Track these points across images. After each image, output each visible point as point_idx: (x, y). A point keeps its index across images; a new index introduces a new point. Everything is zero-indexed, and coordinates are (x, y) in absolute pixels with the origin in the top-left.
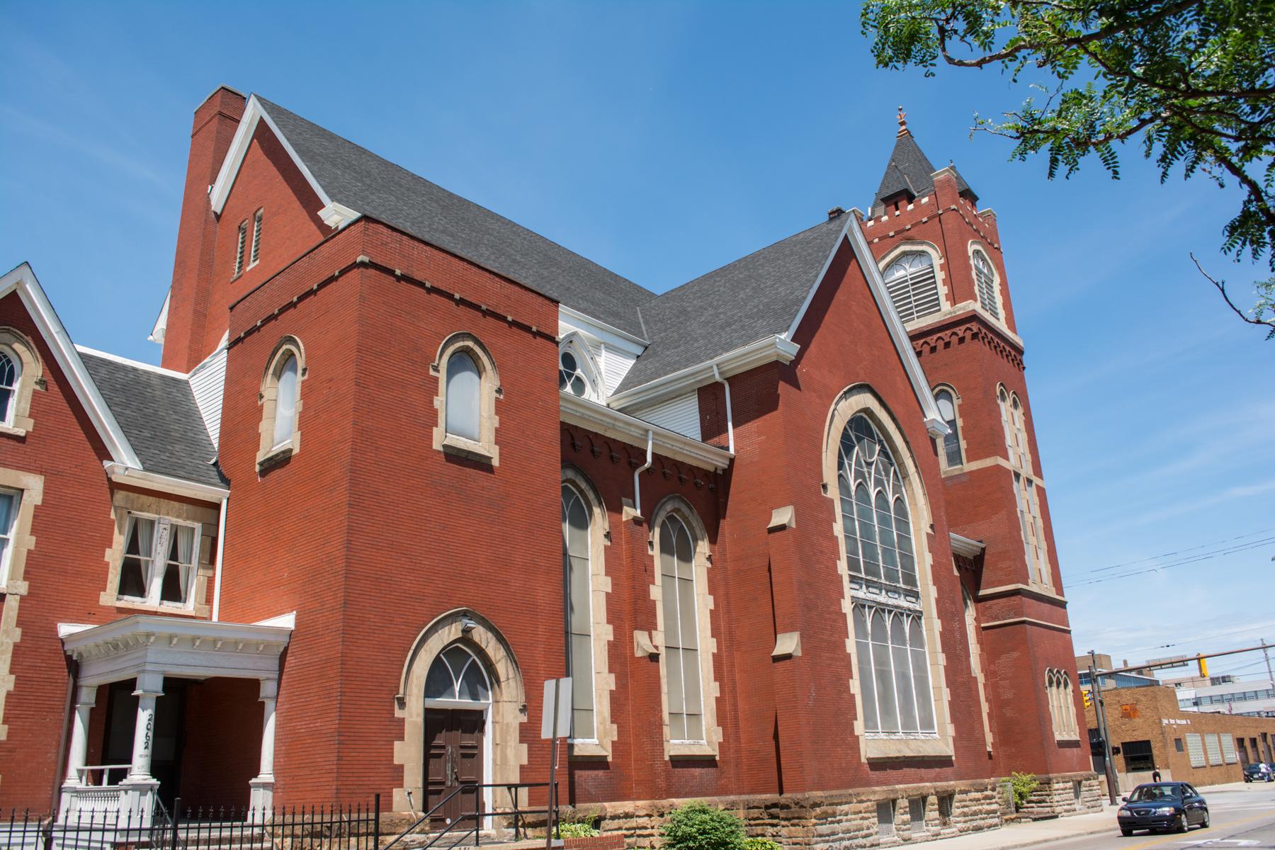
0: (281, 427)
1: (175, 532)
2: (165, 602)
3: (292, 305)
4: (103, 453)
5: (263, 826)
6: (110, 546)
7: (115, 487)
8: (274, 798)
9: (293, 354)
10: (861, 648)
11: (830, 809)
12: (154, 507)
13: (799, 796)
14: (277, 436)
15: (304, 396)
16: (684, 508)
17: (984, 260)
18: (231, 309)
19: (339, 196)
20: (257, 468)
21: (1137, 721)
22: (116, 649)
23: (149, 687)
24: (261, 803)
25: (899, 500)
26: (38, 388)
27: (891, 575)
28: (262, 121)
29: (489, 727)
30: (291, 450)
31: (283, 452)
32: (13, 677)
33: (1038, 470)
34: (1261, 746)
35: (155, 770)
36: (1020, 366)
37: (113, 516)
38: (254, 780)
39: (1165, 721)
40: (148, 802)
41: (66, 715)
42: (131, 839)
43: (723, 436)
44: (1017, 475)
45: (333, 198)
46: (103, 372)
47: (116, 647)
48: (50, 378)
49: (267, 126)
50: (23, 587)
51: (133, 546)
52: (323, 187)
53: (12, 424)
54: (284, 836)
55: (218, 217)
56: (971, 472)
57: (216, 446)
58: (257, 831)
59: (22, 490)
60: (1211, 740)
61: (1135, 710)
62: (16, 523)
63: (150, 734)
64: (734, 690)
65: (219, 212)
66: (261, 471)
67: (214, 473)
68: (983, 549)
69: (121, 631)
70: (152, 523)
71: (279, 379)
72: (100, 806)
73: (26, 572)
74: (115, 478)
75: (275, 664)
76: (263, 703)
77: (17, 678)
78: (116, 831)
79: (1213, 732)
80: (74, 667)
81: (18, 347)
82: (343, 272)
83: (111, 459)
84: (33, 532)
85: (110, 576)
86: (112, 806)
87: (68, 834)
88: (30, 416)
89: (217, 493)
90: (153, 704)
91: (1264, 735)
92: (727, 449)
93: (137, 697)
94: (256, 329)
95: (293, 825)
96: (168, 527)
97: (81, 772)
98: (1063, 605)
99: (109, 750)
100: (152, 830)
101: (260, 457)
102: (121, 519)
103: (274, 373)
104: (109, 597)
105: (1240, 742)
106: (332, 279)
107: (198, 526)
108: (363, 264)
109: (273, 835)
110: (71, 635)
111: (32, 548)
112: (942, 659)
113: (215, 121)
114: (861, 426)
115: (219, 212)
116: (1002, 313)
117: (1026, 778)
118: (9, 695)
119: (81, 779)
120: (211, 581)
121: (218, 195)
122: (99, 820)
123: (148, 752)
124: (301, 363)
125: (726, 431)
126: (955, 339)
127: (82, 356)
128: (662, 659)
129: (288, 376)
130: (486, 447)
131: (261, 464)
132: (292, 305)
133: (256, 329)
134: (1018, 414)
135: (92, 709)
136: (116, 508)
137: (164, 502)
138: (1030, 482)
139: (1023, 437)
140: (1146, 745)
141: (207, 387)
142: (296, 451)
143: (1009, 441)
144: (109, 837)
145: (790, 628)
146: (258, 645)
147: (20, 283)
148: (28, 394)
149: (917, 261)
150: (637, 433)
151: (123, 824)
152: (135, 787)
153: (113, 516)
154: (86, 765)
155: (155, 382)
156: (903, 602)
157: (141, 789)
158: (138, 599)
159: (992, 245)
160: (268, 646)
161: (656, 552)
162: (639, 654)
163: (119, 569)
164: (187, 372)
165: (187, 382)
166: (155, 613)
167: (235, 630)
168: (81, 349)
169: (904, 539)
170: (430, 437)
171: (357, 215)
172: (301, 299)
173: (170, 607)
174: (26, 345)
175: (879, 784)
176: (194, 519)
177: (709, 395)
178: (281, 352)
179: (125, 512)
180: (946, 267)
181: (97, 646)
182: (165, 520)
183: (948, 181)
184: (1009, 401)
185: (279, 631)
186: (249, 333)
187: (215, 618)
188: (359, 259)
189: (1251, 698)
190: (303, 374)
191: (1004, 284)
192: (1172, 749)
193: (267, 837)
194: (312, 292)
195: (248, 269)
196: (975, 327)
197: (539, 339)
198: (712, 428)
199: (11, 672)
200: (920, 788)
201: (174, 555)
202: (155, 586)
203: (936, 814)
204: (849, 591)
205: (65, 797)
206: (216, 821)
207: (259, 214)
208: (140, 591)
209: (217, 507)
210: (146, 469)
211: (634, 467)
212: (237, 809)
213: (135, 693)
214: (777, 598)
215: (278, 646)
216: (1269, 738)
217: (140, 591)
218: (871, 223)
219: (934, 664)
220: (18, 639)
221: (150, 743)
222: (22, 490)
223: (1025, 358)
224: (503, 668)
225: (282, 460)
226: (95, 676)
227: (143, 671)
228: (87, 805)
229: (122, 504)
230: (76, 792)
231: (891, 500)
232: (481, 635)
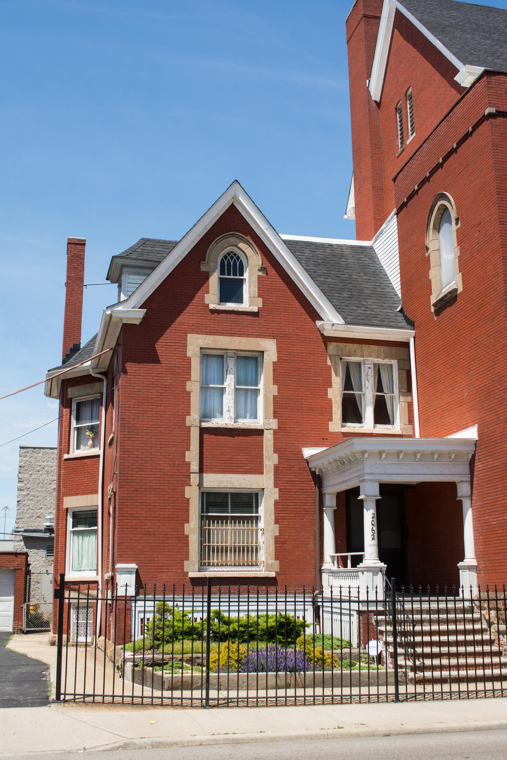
0: (446, 273)
1: (378, 369)
2: (378, 425)
3: (439, 166)
4: (315, 316)
5: (472, 600)
6: (331, 387)
7: (327, 340)
8: (478, 578)
9: (447, 208)
12: (358, 352)
14: (444, 280)
15: (460, 242)
18: (394, 180)
19: (471, 58)
20: (433, 309)
22: (344, 464)
23: (370, 493)
24: (468, 581)
26: (261, 274)
28: (398, 12)
30: (456, 290)
31: (450, 293)
32: (277, 490)
35: (382, 556)
37: (329, 363)
38: (460, 564)
40: (379, 581)
41: (317, 516)
42: (370, 609)
45: (465, 61)
46: (307, 252)
47: (343, 463)
48: (268, 265)
49: (402, 15)
50: (274, 424)
51: (348, 384)
52: (455, 54)
53: (248, 304)
54: (489, 609)
55: (378, 104)
57: (400, 295)
58: (467, 604)
59: (263, 352)
62: (262, 377)
63: (375, 528)
65: (378, 100)
66: (436, 311)
67: (401, 318)
69: (343, 451)
70: (359, 365)
71: (439, 233)
72: (345, 583)
73: (275, 412)
74: (326, 334)
75: (466, 469)
76: (461, 501)
77: (280, 491)
78: (359, 602)
80: (318, 480)
81: (242, 245)
82: (475, 127)
83: (321, 319)
84: (275, 382)
85: (334, 409)
86: (354, 583)
87: (334, 604)
88: (259, 296)
90: (374, 505)
93: (362, 501)
94: (415, 193)
95: (496, 600)
96: (372, 366)
97: (333, 557)
99: (350, 541)
100: (385, 602)
101: (434, 299)
102: (335, 364)
103: (434, 227)
104: (336, 425)
106: (468, 135)
107: (394, 363)
108: (491, 115)
109: (481, 608)
110: (312, 456)
111: (276, 394)
113: (362, 23)
115: (378, 100)
118: (276, 503)
119: (333, 562)
120: (410, 405)
122: (345, 593)
123: (375, 542)
124: (453, 214)
127: (285, 242)
129: (445, 227)
131: (435, 305)
132: (439, 166)
133: (415, 193)
135: (335, 511)
136: (330, 356)
137: (365, 347)
141: (386, 247)
142: (460, 290)
146: (450, 454)
147: (235, 197)
148: (255, 279)
151: (363, 597)
152: (369, 569)
153: (329, 363)
154: (336, 552)
155: (347, 252)
157: (373, 570)
158: (357, 425)
160: (458, 454)
163: (340, 403)
164: (370, 240)
165: (371, 248)
166: (371, 435)
167: (432, 444)
168: (285, 237)
171: (480, 70)
172: (445, 159)
173: (382, 429)
176: (391, 358)
178: (436, 208)
179: (338, 358)
181: (330, 463)
182: (368, 361)
185: (466, 442)
186: (410, 198)
187: (417, 435)
188: (487, 112)
190: (457, 224)
193: (476, 609)
194: (453, 151)
195: (408, 142)
199: (275, 486)
201: (380, 388)
202: (369, 413)
205: (325, 576)
206: (434, 595)
207: (409, 93)
208: (359, 419)
209: (406, 345)
210: (347, 323)
212: (450, 586)
213: (360, 497)
215: (467, 454)
217: (359, 419)
220: (276, 462)
221: (376, 535)
222: (263, 352)
225: (450, 300)
226: (334, 486)
227: (363, 481)
228: (337, 582)
229: (334, 353)
230: (332, 573)
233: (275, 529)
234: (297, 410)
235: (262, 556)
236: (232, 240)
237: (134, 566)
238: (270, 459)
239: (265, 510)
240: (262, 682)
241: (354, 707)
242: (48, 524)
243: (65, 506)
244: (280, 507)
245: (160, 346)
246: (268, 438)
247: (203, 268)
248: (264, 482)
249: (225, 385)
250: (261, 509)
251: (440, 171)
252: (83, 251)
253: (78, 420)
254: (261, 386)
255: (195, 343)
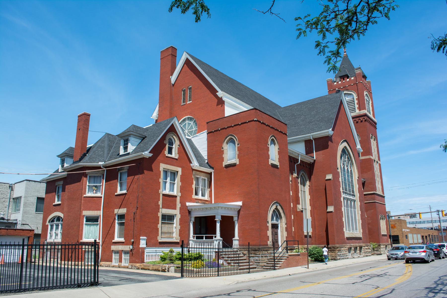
7: (193, 170)
10: (344, 209)
11: (340, 249)
13: (334, 245)
16: (304, 173)
17: (368, 96)
21: (395, 229)
23: (218, 219)
25: (351, 170)
27: (350, 191)
28: (187, 59)
29: (279, 228)
33: (379, 160)
34: (428, 238)
35: (221, 237)
36: (376, 128)
39: (403, 230)
43: (312, 154)
44: (375, 161)
45: (222, 90)
50: (180, 194)
56: (362, 160)
60: (415, 236)
61: (395, 226)
64: (314, 219)
68: (365, 181)
75: (237, 213)
79: (415, 234)
80: (189, 212)
81: (174, 137)
84: (181, 181)
89: (209, 170)
91: (429, 235)
92: (313, 157)
98: (384, 197)
105: (423, 237)
106: (246, 123)
107: (206, 179)
108: (255, 121)
112: (360, 212)
114: (344, 151)
116: (372, 113)
117: (375, 244)
121: (173, 79)
125: (313, 153)
126: (360, 121)
127: (187, 139)
128: (304, 212)
130: (277, 163)
134: (375, 142)
138: (377, 162)
139: (376, 149)
140: (397, 236)
143: (373, 151)
144: (214, 250)
145: (331, 205)
149: (349, 96)
150: (297, 155)
156: (351, 197)
159: (370, 93)
160: (234, 209)
161: (299, 185)
162: (298, 210)
169: (352, 181)
170: (268, 161)
171: (252, 108)
174: (175, 136)
175: (348, 243)
177: (308, 143)
178: (228, 138)
180: (358, 99)
183: (360, 73)
184: (373, 139)
185: (239, 206)
188: (255, 119)
189: (422, 223)
191: (372, 103)
192: (405, 238)
196: (366, 118)
197: (268, 127)
198: (309, 151)
200: (355, 245)
203: (359, 252)
204: (343, 195)
211: (295, 163)
214: (325, 196)
216: (430, 236)
218: (335, 83)
219: (358, 214)
223: (377, 126)
224: (282, 215)
231: (350, 170)
232: (279, 207)
233: (179, 227)
234: (186, 190)
235: (174, 235)
236: (172, 134)
237: (145, 238)
238: (179, 205)
239: (176, 221)
240: (214, 271)
241: (243, 275)
242: (2, 216)
243: (83, 214)
244: (181, 220)
245: (153, 166)
246: (178, 199)
247: (165, 142)
248: (176, 212)
249: (167, 180)
250: (175, 220)
251: (231, 128)
252: (89, 118)
253: (89, 182)
254: (176, 182)
255: (162, 166)
